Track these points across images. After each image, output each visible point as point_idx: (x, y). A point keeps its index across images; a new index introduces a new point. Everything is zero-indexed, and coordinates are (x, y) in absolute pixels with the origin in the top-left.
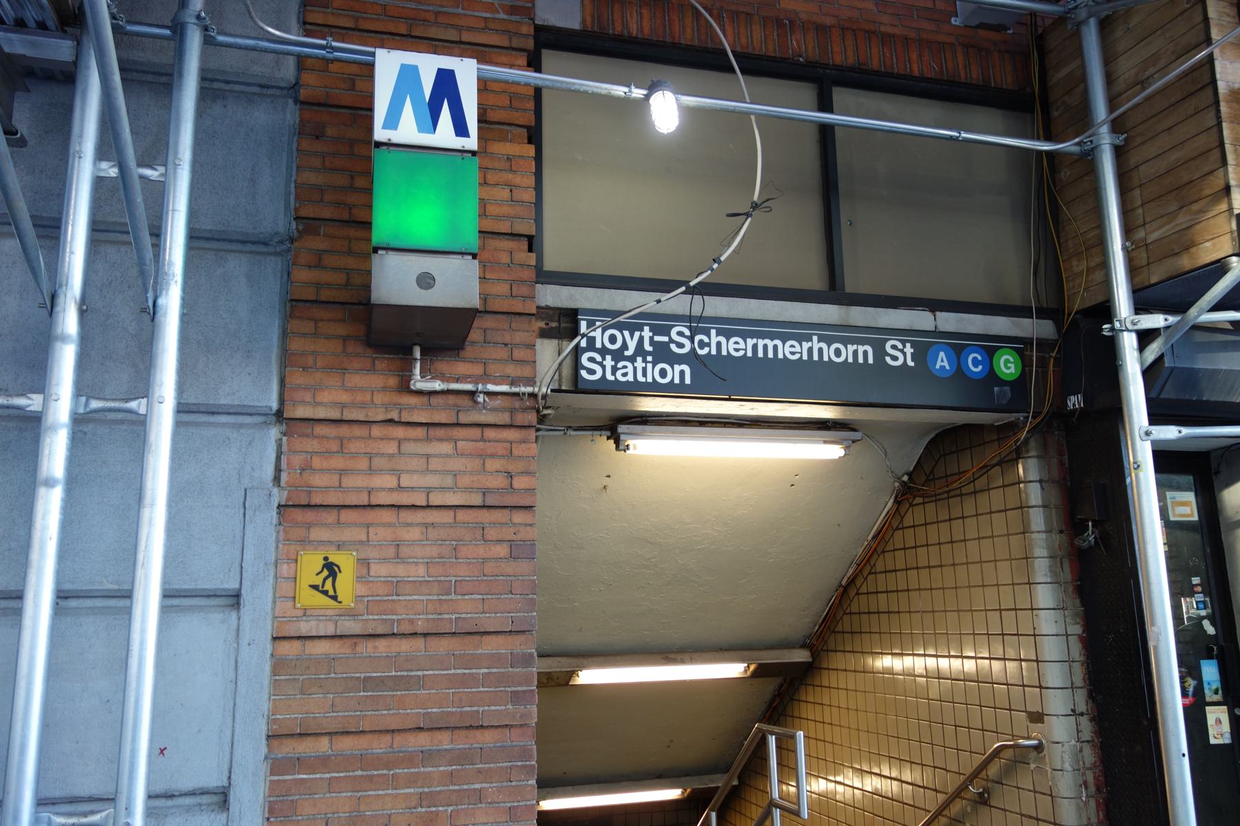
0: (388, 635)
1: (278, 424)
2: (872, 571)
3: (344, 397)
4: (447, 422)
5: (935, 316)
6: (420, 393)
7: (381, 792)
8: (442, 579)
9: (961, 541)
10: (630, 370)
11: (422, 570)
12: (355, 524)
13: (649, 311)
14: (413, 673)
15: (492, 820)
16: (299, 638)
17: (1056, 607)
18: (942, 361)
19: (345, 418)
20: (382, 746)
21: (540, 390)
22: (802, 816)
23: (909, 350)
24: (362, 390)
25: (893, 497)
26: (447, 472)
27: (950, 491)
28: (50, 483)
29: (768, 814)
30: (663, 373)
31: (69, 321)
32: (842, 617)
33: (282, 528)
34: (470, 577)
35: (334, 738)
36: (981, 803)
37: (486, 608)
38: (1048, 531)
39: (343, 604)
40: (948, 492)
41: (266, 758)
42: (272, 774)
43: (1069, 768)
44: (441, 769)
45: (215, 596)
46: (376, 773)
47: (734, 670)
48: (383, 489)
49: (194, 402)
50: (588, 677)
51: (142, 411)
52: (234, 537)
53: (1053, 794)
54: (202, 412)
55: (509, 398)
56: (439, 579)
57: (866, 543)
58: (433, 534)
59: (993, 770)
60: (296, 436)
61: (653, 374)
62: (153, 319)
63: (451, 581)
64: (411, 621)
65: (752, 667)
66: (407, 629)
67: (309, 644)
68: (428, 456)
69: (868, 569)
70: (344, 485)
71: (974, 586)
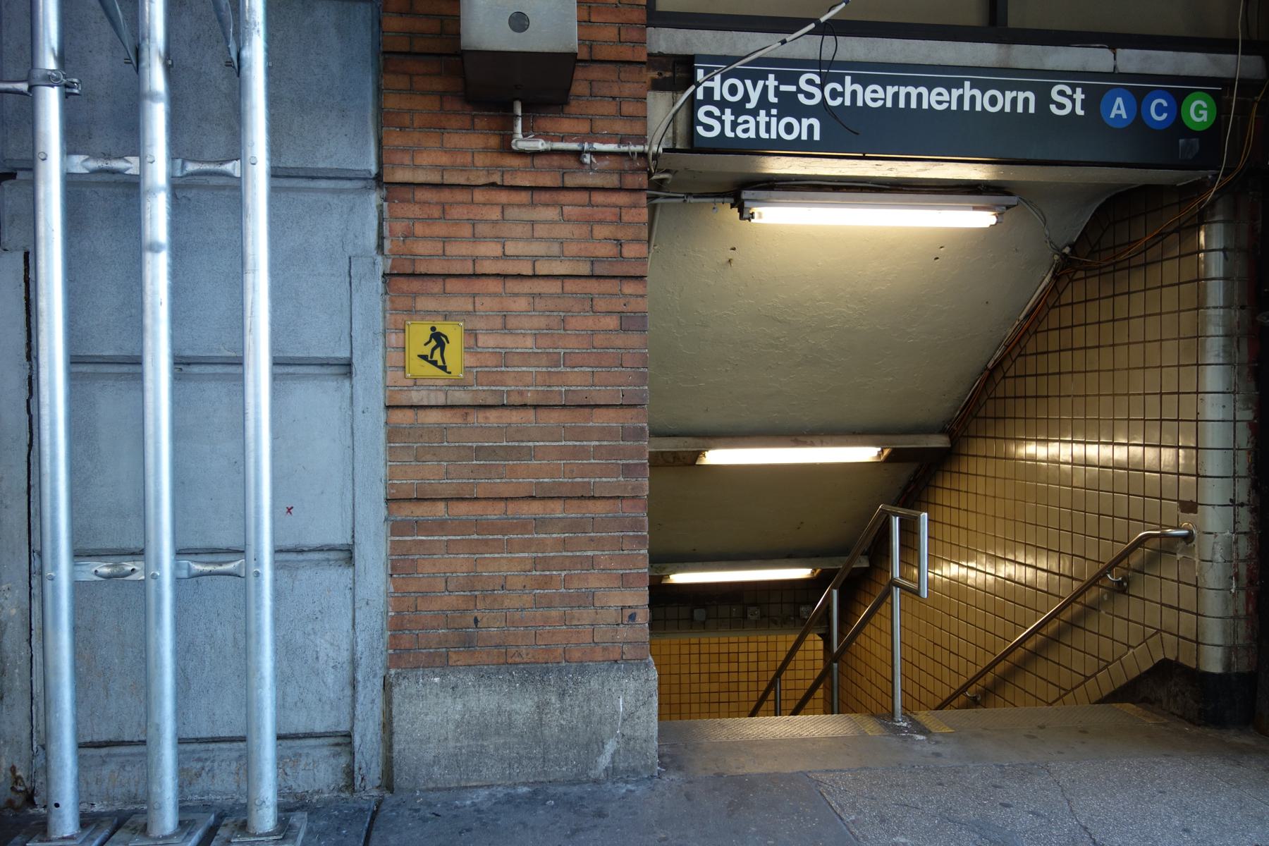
0: (498, 406)
1: (378, 189)
2: (1022, 353)
3: (444, 159)
4: (552, 185)
5: (1115, 54)
6: (522, 153)
7: (496, 555)
8: (551, 350)
9: (1125, 319)
10: (752, 125)
11: (529, 342)
12: (461, 295)
13: (768, 55)
14: (524, 444)
15: (604, 585)
16: (411, 407)
17: (1225, 390)
18: (1119, 108)
19: (445, 182)
20: (496, 512)
21: (650, 149)
22: (922, 595)
23: (1079, 96)
24: (461, 151)
25: (1051, 272)
26: (555, 239)
27: (1117, 262)
28: (155, 248)
29: (888, 593)
30: (789, 128)
31: (157, 78)
32: (985, 402)
33: (388, 297)
34: (579, 349)
35: (449, 503)
36: (1119, 592)
37: (596, 381)
38: (1227, 306)
39: (452, 374)
40: (1114, 264)
41: (386, 520)
42: (392, 535)
43: (1220, 560)
44: (554, 536)
45: (328, 364)
46: (491, 537)
47: (866, 454)
48: (487, 258)
49: (292, 166)
50: (715, 457)
51: (237, 174)
52: (342, 306)
53: (1199, 585)
54: (302, 177)
55: (618, 159)
56: (548, 351)
57: (1017, 323)
58: (540, 304)
59: (1135, 559)
60: (396, 201)
61: (778, 129)
62: (239, 74)
63: (560, 353)
64: (521, 393)
65: (886, 452)
66: (516, 400)
67: (421, 413)
68: (533, 223)
69: (1017, 351)
70: (448, 253)
71: (1134, 368)
